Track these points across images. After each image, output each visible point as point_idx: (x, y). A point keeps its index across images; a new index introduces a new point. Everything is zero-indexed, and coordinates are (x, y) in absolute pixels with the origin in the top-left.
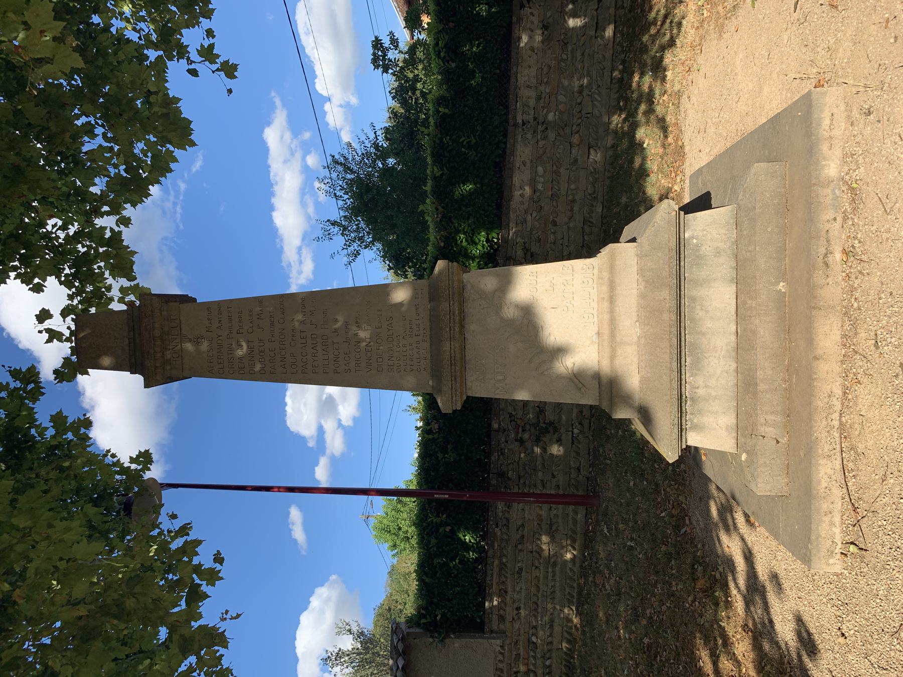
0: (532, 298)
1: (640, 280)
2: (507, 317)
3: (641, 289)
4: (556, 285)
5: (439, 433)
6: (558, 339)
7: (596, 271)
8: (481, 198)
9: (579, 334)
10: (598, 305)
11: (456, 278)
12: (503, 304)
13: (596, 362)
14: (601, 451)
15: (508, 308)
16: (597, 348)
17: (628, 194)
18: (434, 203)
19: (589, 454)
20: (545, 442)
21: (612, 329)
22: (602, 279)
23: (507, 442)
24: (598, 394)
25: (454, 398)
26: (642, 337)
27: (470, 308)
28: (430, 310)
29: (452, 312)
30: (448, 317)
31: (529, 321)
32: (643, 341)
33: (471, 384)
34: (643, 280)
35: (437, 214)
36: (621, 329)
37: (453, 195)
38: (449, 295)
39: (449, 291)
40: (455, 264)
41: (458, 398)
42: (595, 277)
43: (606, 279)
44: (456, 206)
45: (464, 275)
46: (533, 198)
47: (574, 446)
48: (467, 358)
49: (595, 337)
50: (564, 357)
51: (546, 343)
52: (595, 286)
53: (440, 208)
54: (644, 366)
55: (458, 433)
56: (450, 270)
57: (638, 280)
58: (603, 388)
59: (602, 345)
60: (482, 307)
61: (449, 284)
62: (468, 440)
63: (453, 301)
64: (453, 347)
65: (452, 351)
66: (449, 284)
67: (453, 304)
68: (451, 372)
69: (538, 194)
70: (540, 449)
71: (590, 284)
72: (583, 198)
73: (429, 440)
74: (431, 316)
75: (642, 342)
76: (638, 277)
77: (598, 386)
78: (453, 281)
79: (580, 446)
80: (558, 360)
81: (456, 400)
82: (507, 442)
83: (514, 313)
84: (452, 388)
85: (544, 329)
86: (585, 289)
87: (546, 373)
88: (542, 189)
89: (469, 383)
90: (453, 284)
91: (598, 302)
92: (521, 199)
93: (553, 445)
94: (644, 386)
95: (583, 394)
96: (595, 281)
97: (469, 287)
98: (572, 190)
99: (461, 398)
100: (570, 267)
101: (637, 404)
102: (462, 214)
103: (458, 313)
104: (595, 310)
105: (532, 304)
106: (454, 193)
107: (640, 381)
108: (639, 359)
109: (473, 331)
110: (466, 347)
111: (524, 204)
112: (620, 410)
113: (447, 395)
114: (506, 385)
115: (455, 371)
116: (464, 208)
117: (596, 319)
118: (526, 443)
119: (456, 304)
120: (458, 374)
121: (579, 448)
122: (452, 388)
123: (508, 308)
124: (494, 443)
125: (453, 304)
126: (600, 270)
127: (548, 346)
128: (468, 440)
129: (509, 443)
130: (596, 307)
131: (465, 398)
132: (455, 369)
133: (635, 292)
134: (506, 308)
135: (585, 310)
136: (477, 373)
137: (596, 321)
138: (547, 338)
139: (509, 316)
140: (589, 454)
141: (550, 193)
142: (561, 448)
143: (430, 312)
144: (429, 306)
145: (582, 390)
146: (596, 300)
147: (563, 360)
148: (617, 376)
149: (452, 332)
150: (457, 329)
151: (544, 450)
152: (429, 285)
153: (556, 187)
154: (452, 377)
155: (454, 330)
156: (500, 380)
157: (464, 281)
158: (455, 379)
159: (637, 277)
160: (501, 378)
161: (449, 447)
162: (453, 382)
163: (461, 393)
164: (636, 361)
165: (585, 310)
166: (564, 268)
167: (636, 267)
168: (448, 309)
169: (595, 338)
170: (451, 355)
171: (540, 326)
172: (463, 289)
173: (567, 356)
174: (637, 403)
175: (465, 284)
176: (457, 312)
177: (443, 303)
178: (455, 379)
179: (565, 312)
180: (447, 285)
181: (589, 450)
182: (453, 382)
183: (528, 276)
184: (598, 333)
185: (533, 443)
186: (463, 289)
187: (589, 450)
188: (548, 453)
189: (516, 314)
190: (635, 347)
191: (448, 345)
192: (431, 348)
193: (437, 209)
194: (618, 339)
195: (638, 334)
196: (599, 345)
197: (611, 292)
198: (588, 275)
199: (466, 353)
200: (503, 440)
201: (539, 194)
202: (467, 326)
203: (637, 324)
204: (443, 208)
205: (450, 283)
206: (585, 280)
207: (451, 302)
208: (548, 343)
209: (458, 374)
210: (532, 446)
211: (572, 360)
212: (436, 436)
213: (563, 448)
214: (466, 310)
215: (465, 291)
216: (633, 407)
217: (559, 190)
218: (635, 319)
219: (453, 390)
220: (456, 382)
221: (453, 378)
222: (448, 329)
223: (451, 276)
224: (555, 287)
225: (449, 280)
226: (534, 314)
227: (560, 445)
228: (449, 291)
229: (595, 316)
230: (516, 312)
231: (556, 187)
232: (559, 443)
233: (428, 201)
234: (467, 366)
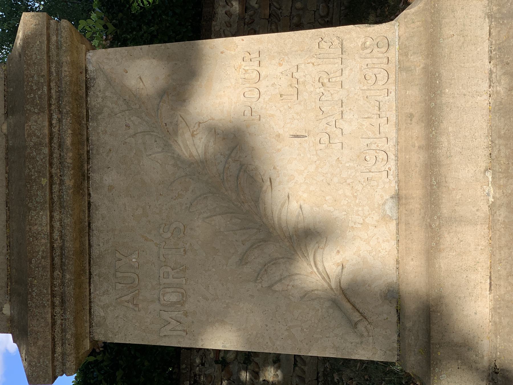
0: (248, 113)
1: (498, 72)
2: (191, 155)
3: (498, 93)
4: (304, 83)
5: (104, 353)
6: (307, 208)
7: (394, 53)
8: (171, 13)
9: (355, 197)
10: (398, 130)
11: (66, 58)
12: (182, 125)
13: (391, 263)
14: (336, 378)
15: (193, 135)
16: (395, 231)
17: (379, 11)
18: (102, 19)
19: (317, 379)
20: (257, 364)
21: (431, 185)
22: (407, 70)
23: (203, 364)
24: (395, 337)
25: (59, 350)
26: (500, 206)
27: (105, 132)
28: (6, 136)
29: (55, 140)
30: (46, 151)
31: (242, 165)
32: (502, 214)
33: (102, 314)
34: (504, 74)
35: (106, 36)
36: (452, 186)
37: (129, 8)
38: (50, 98)
39: (49, 89)
40: (65, 23)
41: (69, 349)
42: (392, 67)
43: (418, 71)
44: (134, 24)
45: (90, 54)
46: (244, 18)
47: (297, 368)
48: (95, 252)
49: (390, 204)
50: (320, 251)
51: (280, 219)
52: (392, 88)
53: (109, 25)
54: (504, 273)
55: (133, 353)
56: (54, 38)
57: (491, 72)
58: (409, 324)
59: (407, 224)
60: (131, 131)
61: (50, 72)
62: (146, 363)
63: (60, 112)
64: (57, 225)
65: (56, 235)
66: (50, 72)
67: (60, 121)
68: (53, 285)
69: (251, 12)
70: (250, 373)
71: (380, 83)
72: (313, 21)
73: (90, 363)
74: (8, 150)
75: (501, 219)
76: (491, 66)
77: (395, 319)
78: (59, 64)
79: (306, 368)
80: (305, 256)
81: (63, 354)
82: (203, 364)
83: (206, 147)
84: (54, 323)
85: (275, 184)
86: (368, 93)
87: (278, 287)
88: (256, 6)
89: (98, 312)
90: (58, 73)
91: (398, 125)
92: (227, 18)
93: (269, 368)
94: (505, 321)
95: (362, 336)
96: (392, 76)
97: (100, 83)
98: (298, 10)
99: (77, 347)
100: (336, 42)
101: (485, 362)
102: (143, 35)
103: (73, 144)
104: (392, 143)
105: (248, 126)
106: (131, 5)
107: (494, 309)
108: (492, 254)
109: (111, 188)
110: (93, 226)
111: (231, 26)
112: (448, 376)
113: (40, 343)
114: (186, 314)
115: (63, 284)
116: (145, 27)
117: (392, 164)
118: (231, 366)
119: (67, 121)
120: (70, 290)
121: (304, 372)
122: (54, 323)
123: (193, 135)
124: (184, 366)
125: (60, 121)
126: (404, 51)
127: (284, 225)
128: (146, 363)
129: (207, 365)
130: (393, 135)
131: (87, 345)
132: (63, 276)
133: (483, 101)
134: (188, 135)
135: (368, 141)
136: (120, 286)
137: (393, 168)
138: (283, 205)
139: (195, 153)
140: (317, 379)
141: (267, 12)
142: (279, 372)
143: (7, 140)
144: (5, 127)
145: (361, 327)
146: (393, 119)
147: (318, 258)
148: (440, 298)
149: (56, 188)
150: (69, 182)
151: (256, 374)
152: (6, 78)
153: (275, 4)
154: (53, 296)
155: (62, 183)
156: (173, 304)
157: (90, 68)
158: (63, 302)
159: (488, 66)
160: (173, 298)
161: (117, 374)
162: (58, 309)
163: (78, 338)
164: (484, 259)
165: (368, 141)
166: (323, 45)
167: (486, 44)
168: (46, 131)
169: (390, 208)
170: (52, 243)
171: (266, 178)
172: (87, 88)
173: (327, 249)
174: (486, 358)
175: (91, 74)
176: (68, 141)
177: (34, 117)
178: (63, 302)
179: (322, 146)
180: (45, 72)
181: (318, 373)
182: (58, 309)
183: (240, 60)
184: (398, 197)
185: (241, 365)
186: (87, 88)
187: (318, 373)
188: (261, 379)
189: (211, 150)
190: (482, 230)
191: (46, 219)
192: (8, 227)
193: (105, 27)
194: (445, 211)
195: (491, 199)
196: (398, 224)
197: (431, 99)
198: (375, 61)
199: (94, 241)
200: (198, 361)
201: (252, 12)
202: (95, 176)
203: (489, 175)
204: (115, 25)
205: (53, 70)
206: (370, 74)
207: (55, 116)
208: (283, 217)
209: (70, 290)
210: (239, 371)
211: (338, 258)
212: (99, 358)
213: (282, 372)
214: (93, 138)
215: (91, 93)
216: (477, 369)
217: (279, 9)
218: (483, 162)
219: (58, 329)
220: (64, 310)
221: (57, 302)
222: (45, 181)
223: (53, 51)
224: (301, 88)
225: (49, 62)
226: (253, 149)
227: (278, 368)
228: (49, 89)
229: (392, 157)
230: (211, 144)
231: (275, 4)
232: (276, 365)
233: (94, 16)
234: (95, 271)
